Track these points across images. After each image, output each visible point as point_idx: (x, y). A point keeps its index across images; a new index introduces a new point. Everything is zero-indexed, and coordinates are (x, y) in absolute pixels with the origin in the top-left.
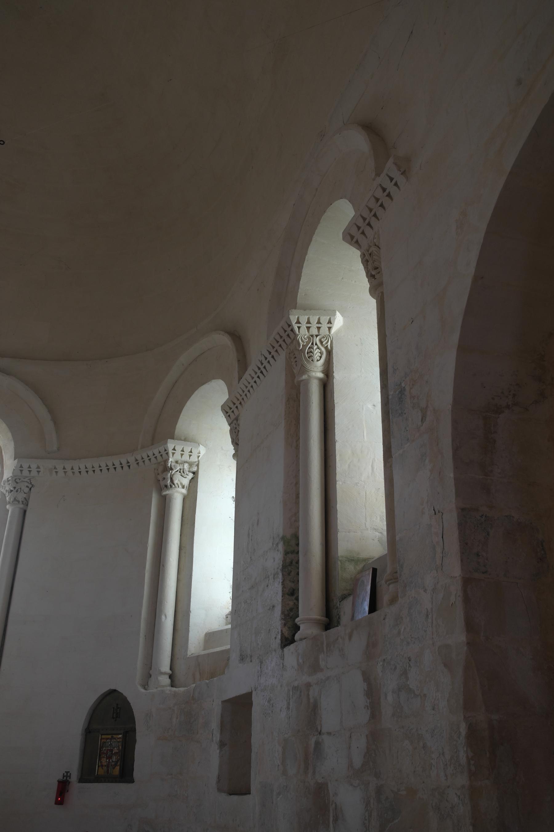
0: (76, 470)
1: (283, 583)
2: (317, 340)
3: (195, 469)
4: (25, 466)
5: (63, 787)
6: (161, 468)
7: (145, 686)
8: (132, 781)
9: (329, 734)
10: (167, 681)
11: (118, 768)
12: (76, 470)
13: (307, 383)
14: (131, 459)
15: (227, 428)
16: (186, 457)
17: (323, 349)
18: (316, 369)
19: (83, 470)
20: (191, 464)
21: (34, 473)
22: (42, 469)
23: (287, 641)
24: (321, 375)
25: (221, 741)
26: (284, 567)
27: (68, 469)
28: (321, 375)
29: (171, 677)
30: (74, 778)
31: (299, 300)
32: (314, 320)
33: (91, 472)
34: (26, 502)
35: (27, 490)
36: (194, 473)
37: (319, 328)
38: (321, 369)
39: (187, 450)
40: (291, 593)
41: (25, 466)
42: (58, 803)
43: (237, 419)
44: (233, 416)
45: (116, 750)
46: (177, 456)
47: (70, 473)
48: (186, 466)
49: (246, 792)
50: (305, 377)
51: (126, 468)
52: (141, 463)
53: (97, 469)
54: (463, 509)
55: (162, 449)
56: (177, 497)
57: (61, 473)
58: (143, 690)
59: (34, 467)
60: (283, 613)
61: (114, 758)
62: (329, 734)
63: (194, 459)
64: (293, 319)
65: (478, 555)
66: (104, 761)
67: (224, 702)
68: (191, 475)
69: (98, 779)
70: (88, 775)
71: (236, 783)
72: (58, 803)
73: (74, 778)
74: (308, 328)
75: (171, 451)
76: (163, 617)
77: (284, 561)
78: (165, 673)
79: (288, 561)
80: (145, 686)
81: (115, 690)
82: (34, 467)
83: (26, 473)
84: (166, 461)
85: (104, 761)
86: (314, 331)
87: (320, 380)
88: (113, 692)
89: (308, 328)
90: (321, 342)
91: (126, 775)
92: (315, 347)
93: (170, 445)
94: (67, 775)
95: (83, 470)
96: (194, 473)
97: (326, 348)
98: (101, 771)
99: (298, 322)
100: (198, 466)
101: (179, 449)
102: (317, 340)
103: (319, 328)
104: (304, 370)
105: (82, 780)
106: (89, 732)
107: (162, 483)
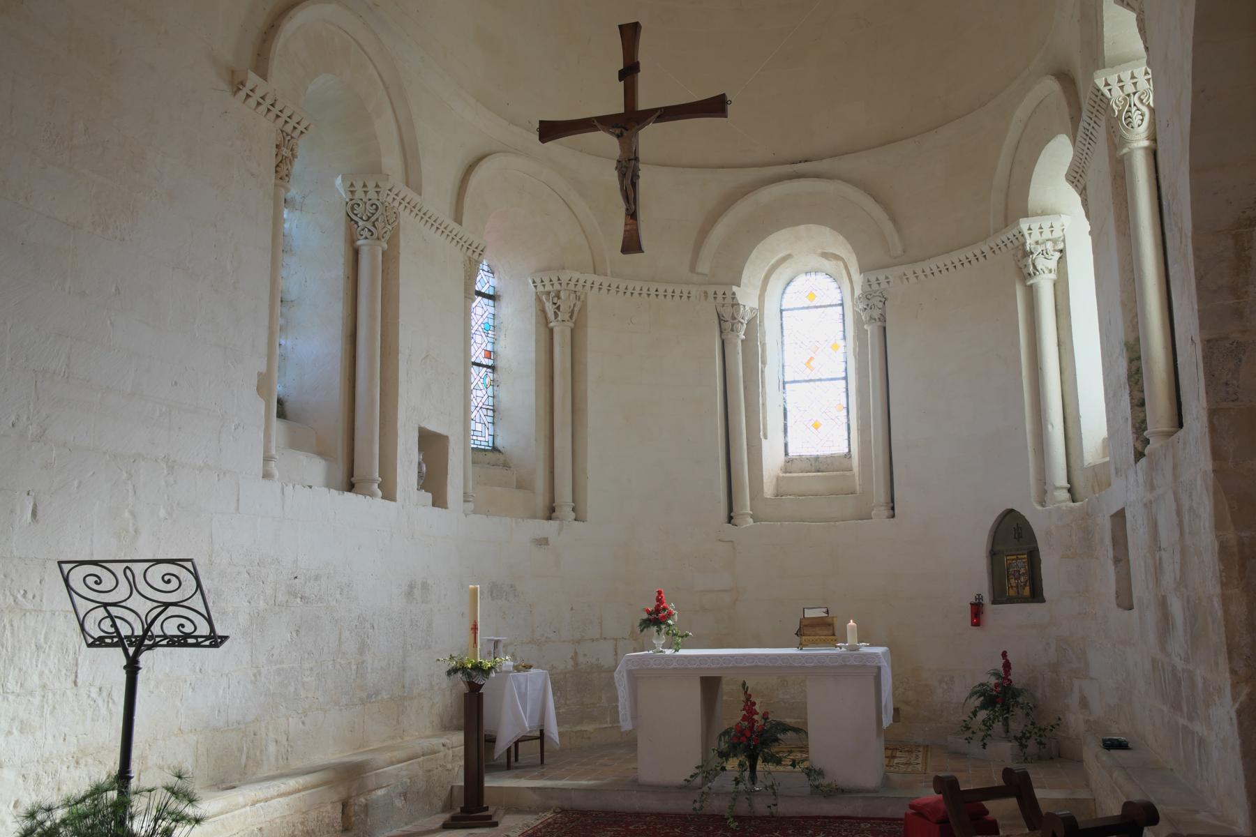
0: (928, 272)
1: (1131, 395)
2: (1135, 99)
3: (1061, 246)
4: (873, 279)
5: (977, 611)
6: (1020, 254)
7: (1042, 503)
8: (1043, 601)
9: (629, 72)
10: (1066, 495)
11: (1027, 588)
12: (928, 272)
13: (1130, 155)
14: (986, 248)
15: (1078, 199)
16: (1047, 235)
17: (1145, 109)
18: (1138, 137)
19: (936, 270)
20: (1055, 241)
21: (884, 285)
22: (891, 279)
23: (1139, 455)
24: (1145, 143)
25: (1115, 557)
26: (1130, 377)
27: (919, 272)
28: (1145, 143)
29: (1069, 491)
30: (987, 599)
31: (1109, 51)
32: (1126, 76)
33: (944, 272)
34: (883, 318)
35: (881, 305)
36: (1061, 251)
37: (1135, 84)
38: (1145, 135)
39: (1046, 226)
40: (1139, 404)
41: (873, 279)
42: (974, 624)
43: (1085, 188)
44: (1081, 187)
45: (1022, 571)
46: (1036, 235)
47: (922, 276)
48: (1049, 245)
49: (1131, 608)
50: (1125, 151)
51: (981, 259)
52: (997, 251)
53: (951, 267)
54: (1209, 341)
55: (1015, 231)
56: (1045, 284)
57: (912, 279)
58: (1039, 508)
59: (882, 278)
60: (1133, 426)
61: (1022, 579)
62: (629, 72)
63: (1057, 234)
64: (1100, 82)
65: (1227, 384)
66: (1013, 581)
67: (1112, 516)
68: (1058, 255)
69: (1011, 600)
70: (1000, 596)
71: (1125, 600)
72: (974, 624)
73: (987, 599)
74: (1122, 87)
75: (1026, 233)
76: (1050, 427)
77: (1129, 369)
78: (1062, 488)
79: (1134, 369)
80: (1042, 503)
81: (1012, 510)
82: (882, 278)
83: (875, 287)
84: (1024, 244)
85: (1013, 581)
86: (1129, 89)
87: (1146, 148)
88: (1010, 512)
89: (1122, 87)
90: (1141, 100)
91: (1036, 595)
92: (1134, 109)
93: (1024, 225)
94: (979, 597)
95: (936, 270)
96: (1061, 251)
97: (1148, 106)
98: (1012, 593)
99: (1107, 84)
100: (1064, 241)
101: (1035, 227)
102: (1135, 99)
103: (1135, 84)
104: (1124, 142)
105: (994, 602)
106: (994, 554)
107: (1025, 271)
